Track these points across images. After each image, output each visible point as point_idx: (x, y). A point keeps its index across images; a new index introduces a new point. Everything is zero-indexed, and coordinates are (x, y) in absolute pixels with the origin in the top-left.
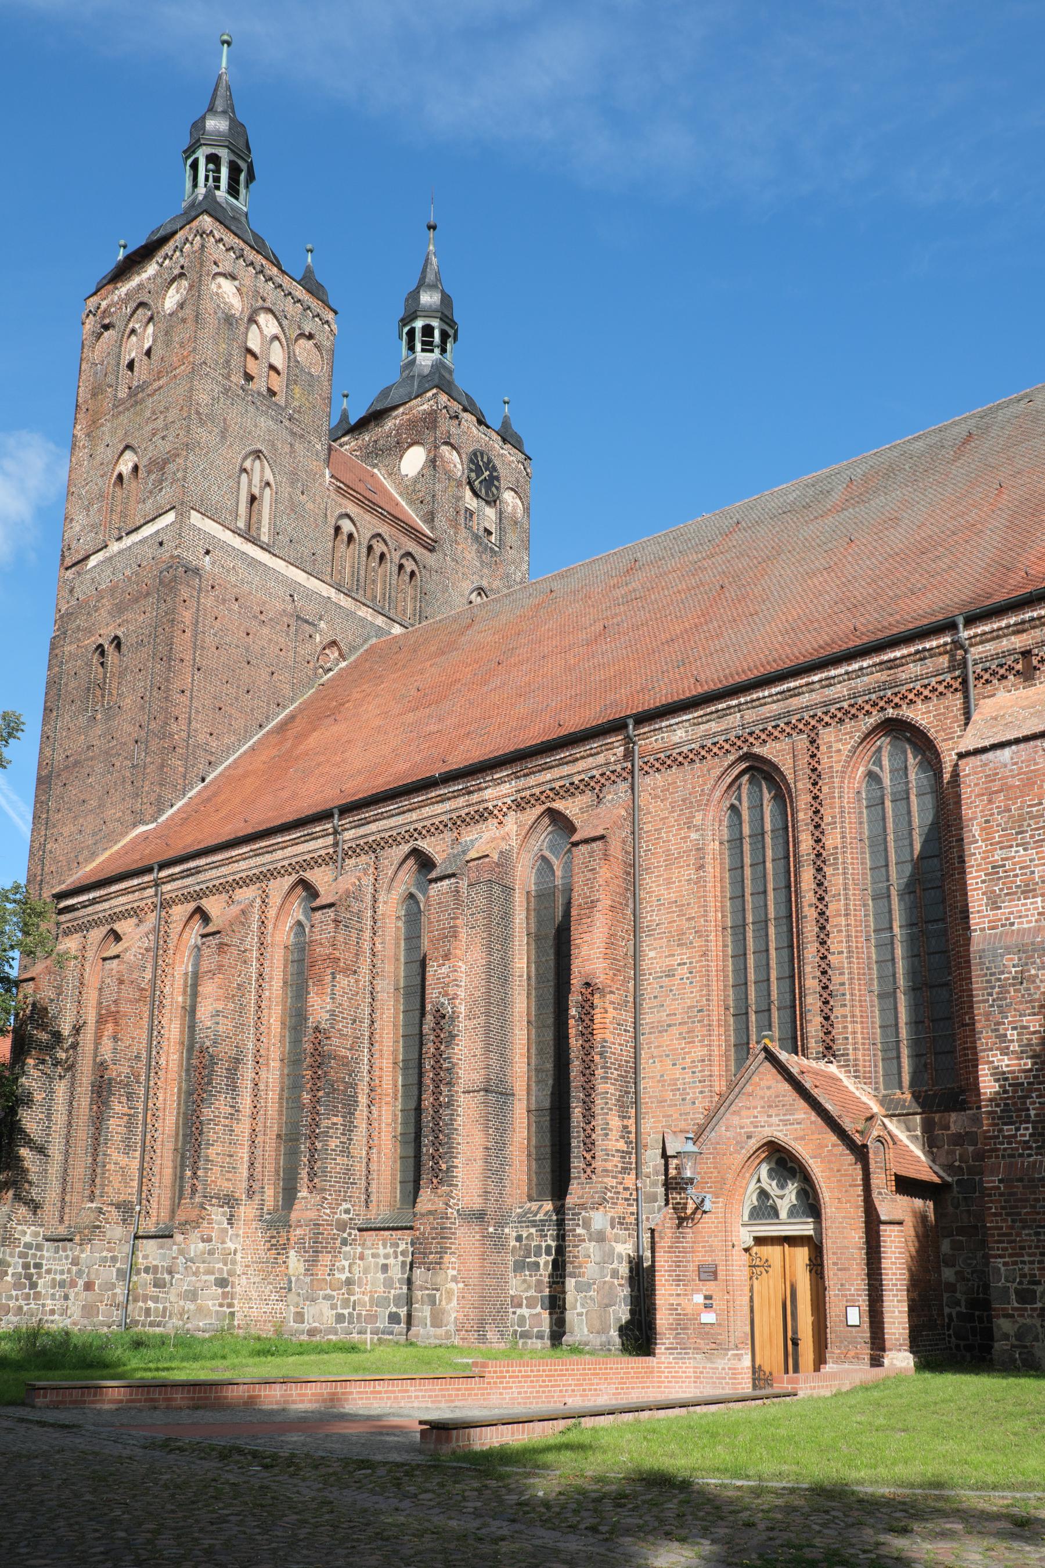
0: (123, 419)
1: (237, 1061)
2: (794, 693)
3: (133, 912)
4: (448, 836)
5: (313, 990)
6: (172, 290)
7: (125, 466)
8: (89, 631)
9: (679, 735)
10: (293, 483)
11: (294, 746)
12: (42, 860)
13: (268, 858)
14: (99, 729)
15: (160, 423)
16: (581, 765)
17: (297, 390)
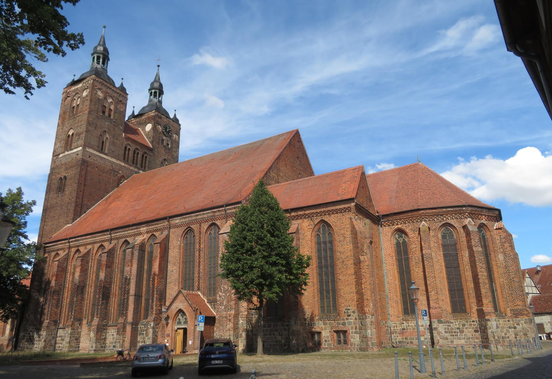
0: (71, 121)
1: (84, 287)
2: (198, 215)
3: (62, 249)
4: (133, 238)
5: (101, 271)
6: (85, 92)
7: (70, 133)
8: (59, 174)
9: (177, 221)
10: (114, 137)
11: (108, 206)
12: (43, 230)
13: (95, 239)
14: (59, 199)
15: (79, 124)
16: (159, 225)
17: (116, 115)
